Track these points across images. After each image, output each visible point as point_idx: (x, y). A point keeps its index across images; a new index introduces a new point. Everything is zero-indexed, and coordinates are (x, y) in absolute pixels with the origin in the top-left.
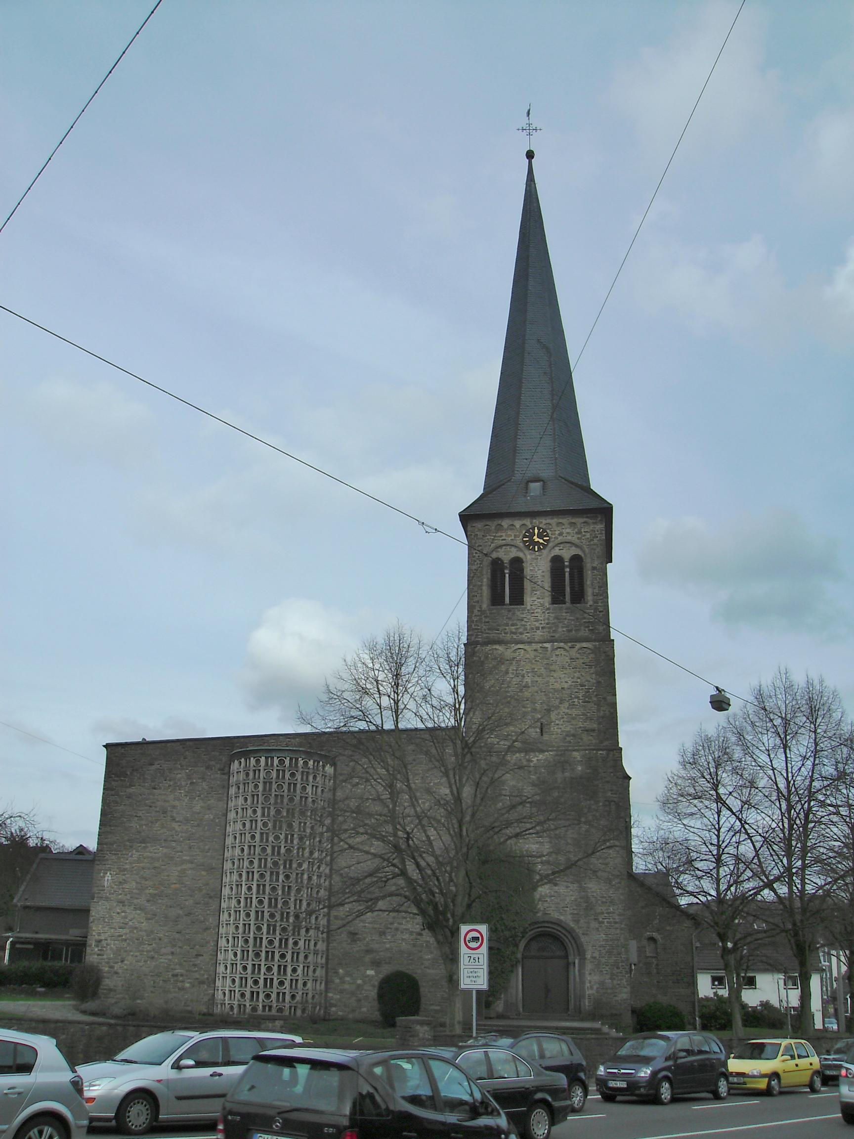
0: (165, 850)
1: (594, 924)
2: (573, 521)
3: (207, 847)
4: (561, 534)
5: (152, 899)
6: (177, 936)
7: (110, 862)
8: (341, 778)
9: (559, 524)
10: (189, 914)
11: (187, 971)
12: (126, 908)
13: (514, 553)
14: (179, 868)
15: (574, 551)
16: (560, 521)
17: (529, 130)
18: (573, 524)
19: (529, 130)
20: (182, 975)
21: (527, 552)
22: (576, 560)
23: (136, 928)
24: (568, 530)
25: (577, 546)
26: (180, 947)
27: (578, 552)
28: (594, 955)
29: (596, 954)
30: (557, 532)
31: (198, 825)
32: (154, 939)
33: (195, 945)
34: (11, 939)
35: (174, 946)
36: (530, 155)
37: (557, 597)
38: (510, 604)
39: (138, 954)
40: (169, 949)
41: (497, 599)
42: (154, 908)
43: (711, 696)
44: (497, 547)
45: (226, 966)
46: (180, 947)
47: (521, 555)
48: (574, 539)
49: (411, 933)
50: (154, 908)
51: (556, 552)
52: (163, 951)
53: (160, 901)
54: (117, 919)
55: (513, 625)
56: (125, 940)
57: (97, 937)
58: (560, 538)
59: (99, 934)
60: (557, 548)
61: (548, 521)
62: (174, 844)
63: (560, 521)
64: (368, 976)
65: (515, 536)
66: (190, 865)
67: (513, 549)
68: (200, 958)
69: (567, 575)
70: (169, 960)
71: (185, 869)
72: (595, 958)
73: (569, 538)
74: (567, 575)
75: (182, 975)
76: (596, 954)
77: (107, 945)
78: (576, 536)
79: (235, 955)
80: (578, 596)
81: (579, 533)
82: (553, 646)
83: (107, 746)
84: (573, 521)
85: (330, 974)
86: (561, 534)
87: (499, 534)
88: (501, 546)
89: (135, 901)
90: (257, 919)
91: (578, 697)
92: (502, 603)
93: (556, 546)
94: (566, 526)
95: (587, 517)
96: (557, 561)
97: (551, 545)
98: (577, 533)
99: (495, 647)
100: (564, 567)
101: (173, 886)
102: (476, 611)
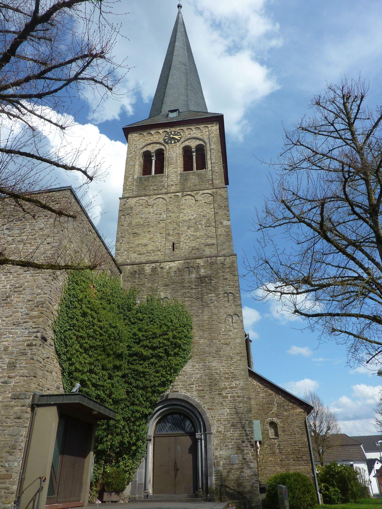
1: (218, 399)
15: (198, 142)
28: (220, 429)
29: (221, 429)
30: (187, 133)
36: (179, 6)
47: (163, 147)
72: (220, 432)
76: (221, 429)
82: (183, 194)
86: (189, 134)
91: (201, 224)
99: (141, 198)
100: (192, 152)
102: (130, 179)
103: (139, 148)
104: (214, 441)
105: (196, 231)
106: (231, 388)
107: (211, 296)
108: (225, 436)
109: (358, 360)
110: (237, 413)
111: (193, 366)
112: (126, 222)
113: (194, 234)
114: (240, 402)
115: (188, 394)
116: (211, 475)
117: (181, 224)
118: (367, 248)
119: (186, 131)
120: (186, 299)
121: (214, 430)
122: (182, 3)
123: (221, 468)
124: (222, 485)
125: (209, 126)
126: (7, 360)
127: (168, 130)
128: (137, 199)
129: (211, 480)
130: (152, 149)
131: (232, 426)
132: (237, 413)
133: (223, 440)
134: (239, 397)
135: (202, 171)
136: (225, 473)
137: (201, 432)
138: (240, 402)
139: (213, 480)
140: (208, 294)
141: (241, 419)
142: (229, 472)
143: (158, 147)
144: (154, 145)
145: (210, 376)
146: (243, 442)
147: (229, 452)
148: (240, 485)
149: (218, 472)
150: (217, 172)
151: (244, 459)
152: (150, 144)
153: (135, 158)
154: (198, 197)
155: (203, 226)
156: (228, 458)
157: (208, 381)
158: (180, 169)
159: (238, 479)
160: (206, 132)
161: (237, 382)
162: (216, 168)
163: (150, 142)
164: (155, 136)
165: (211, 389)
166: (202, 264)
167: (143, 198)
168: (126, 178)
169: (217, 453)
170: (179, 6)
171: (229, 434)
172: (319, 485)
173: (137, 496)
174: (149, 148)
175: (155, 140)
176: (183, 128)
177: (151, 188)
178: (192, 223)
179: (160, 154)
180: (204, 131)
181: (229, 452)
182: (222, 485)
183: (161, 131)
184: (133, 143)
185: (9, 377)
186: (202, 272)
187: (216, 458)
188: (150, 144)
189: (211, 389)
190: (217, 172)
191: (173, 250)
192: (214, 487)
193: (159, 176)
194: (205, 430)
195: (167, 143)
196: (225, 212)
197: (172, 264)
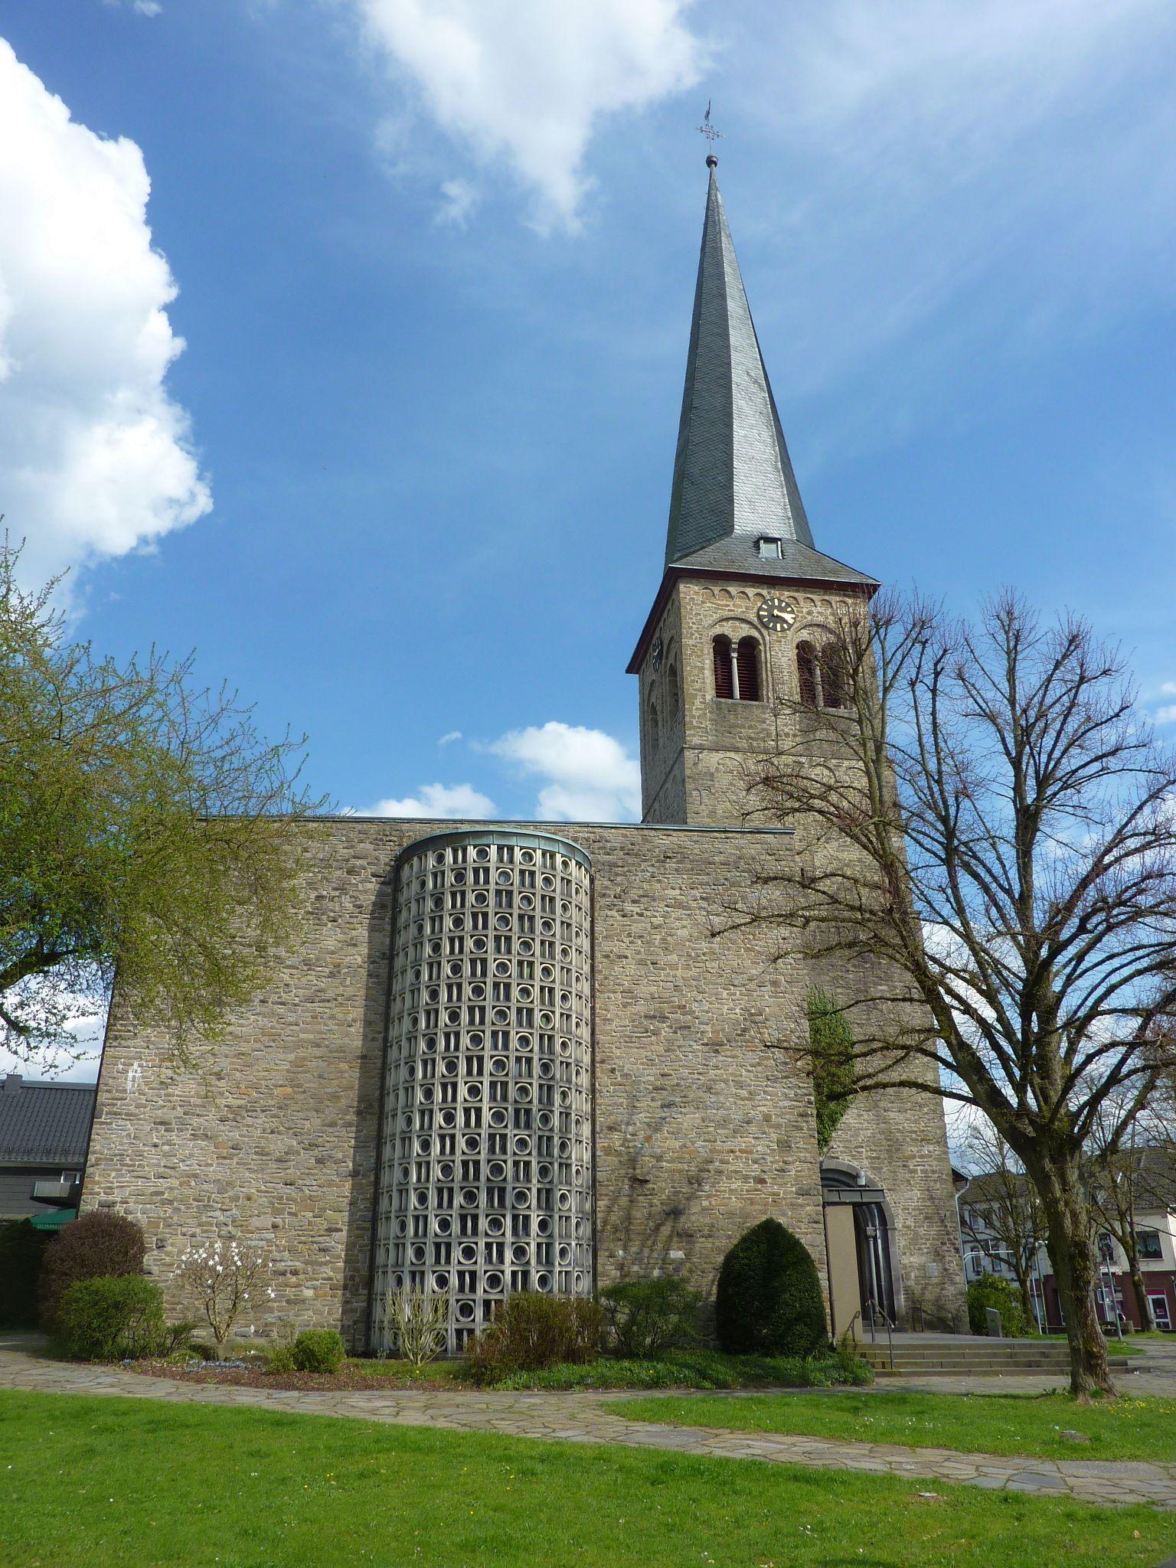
0: (262, 1021)
1: (902, 1174)
3: (350, 1017)
5: (232, 1117)
6: (288, 1190)
8: (603, 901)
10: (313, 1146)
11: (306, 1263)
12: (173, 1136)
14: (291, 1057)
17: (711, 134)
20: (295, 1273)
22: (831, 650)
23: (195, 1176)
28: (908, 1223)
29: (910, 1222)
31: (332, 975)
32: (236, 1199)
33: (324, 1210)
35: (277, 1212)
36: (710, 162)
39: (198, 1230)
40: (268, 1221)
42: (236, 1135)
47: (756, 634)
49: (746, 1178)
50: (236, 1135)
52: (255, 1222)
53: (249, 1121)
54: (152, 1156)
56: (171, 1202)
57: (103, 1197)
59: (109, 1191)
62: (281, 1009)
64: (674, 1261)
66: (316, 1052)
70: (268, 1241)
71: (304, 1059)
72: (908, 1227)
73: (821, 619)
75: (295, 1273)
76: (910, 1222)
83: (628, 671)
85: (600, 1261)
86: (810, 613)
89: (195, 1121)
90: (492, 1150)
92: (731, 696)
94: (819, 604)
96: (804, 648)
99: (729, 754)
103: (705, 624)
104: (899, 1242)
106: (922, 1157)
108: (916, 1233)
110: (932, 1198)
111: (860, 1116)
112: (703, 807)
114: (935, 1181)
115: (855, 1164)
116: (899, 1291)
118: (1046, 849)
119: (802, 604)
120: (839, 990)
121: (899, 1225)
123: (911, 1283)
124: (916, 1308)
125: (850, 601)
126: (774, 1137)
127: (764, 592)
128: (721, 755)
130: (737, 633)
131: (926, 1218)
132: (932, 1198)
133: (915, 1240)
134: (934, 1172)
136: (918, 1290)
137: (874, 1225)
138: (935, 1181)
139: (901, 1301)
140: (876, 984)
141: (938, 1208)
142: (923, 1289)
143: (745, 631)
144: (737, 624)
145: (888, 1135)
146: (944, 1244)
147: (924, 1259)
148: (941, 1308)
149: (907, 1289)
151: (946, 1270)
152: (728, 619)
153: (702, 651)
156: (922, 1267)
157: (884, 1142)
159: (938, 1299)
161: (931, 1148)
163: (727, 614)
164: (738, 602)
165: (891, 1157)
167: (732, 755)
169: (905, 1260)
171: (922, 1231)
174: (726, 629)
175: (738, 612)
176: (796, 595)
177: (745, 732)
179: (749, 647)
181: (924, 1259)
182: (916, 1308)
183: (751, 591)
185: (785, 1162)
187: (905, 1267)
188: (728, 619)
189: (891, 1157)
192: (903, 1311)
193: (757, 707)
194: (884, 1221)
195: (767, 628)
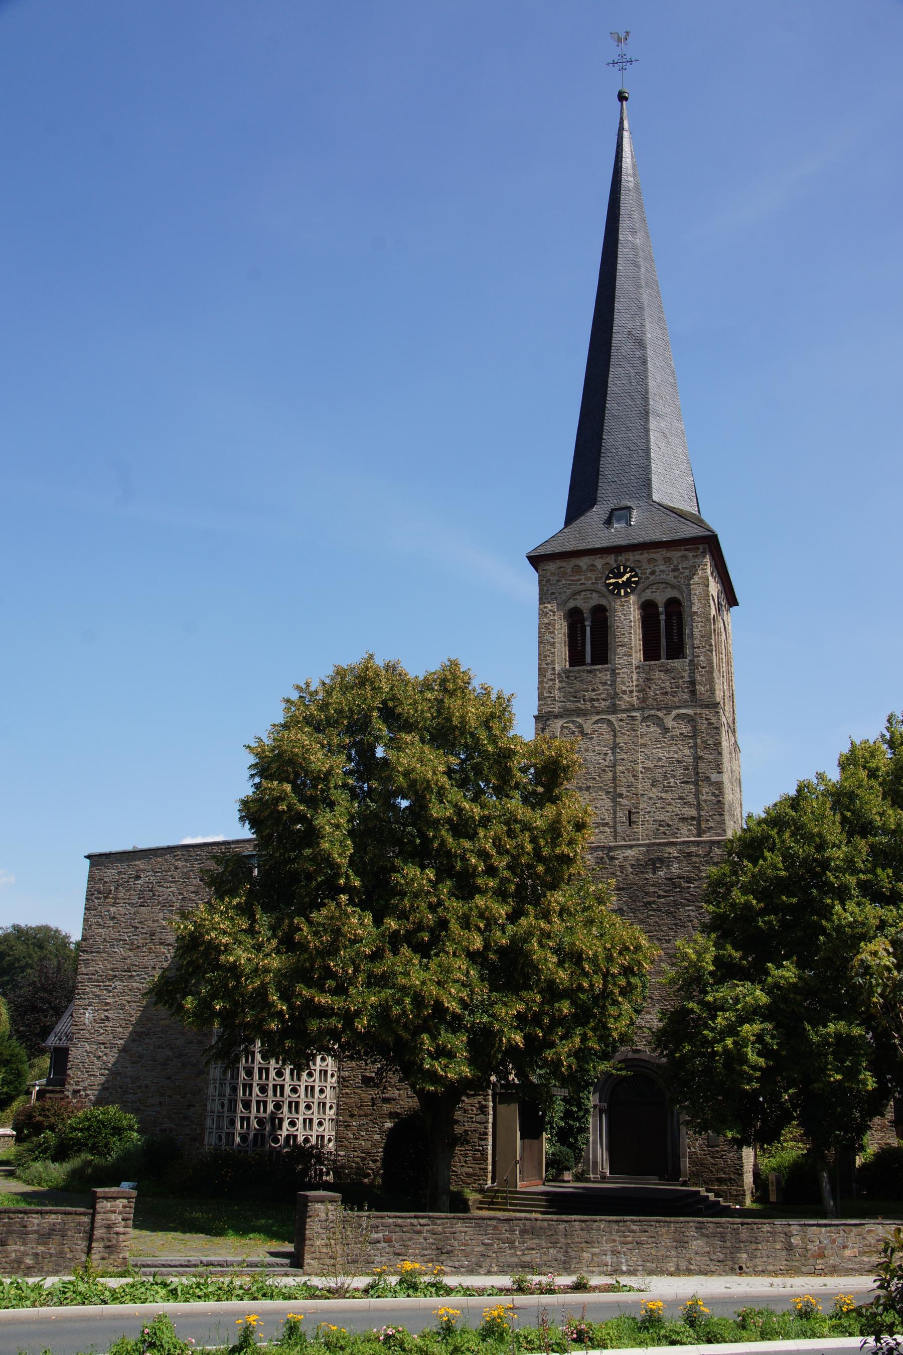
2: (669, 555)
4: (652, 573)
7: (91, 995)
9: (650, 561)
13: (595, 600)
15: (671, 593)
16: (652, 556)
18: (668, 560)
19: (622, 63)
21: (611, 597)
23: (120, 1074)
24: (662, 568)
25: (673, 587)
26: (170, 1096)
27: (675, 594)
30: (648, 571)
32: (140, 1087)
34: (37, 1088)
36: (622, 97)
37: (651, 652)
38: (593, 663)
41: (576, 658)
43: (245, 803)
44: (575, 594)
45: (213, 1119)
46: (170, 1096)
47: (604, 602)
48: (670, 577)
51: (648, 595)
53: (147, 1041)
55: (593, 690)
58: (652, 577)
60: (648, 591)
61: (638, 557)
63: (652, 556)
65: (596, 579)
67: (595, 595)
68: (192, 1109)
69: (662, 623)
73: (663, 576)
74: (662, 623)
77: (87, 1095)
78: (672, 574)
79: (223, 1105)
80: (677, 650)
81: (676, 569)
82: (642, 715)
84: (669, 555)
87: (577, 577)
88: (579, 593)
91: (674, 777)
93: (647, 588)
95: (686, 550)
97: (640, 586)
98: (673, 570)
100: (658, 614)
101: (162, 1022)
102: (549, 675)
105: (667, 791)
107: (689, 910)
109: (403, 1282)
113: (663, 795)
117: (640, 775)
122: (629, 91)
129: (685, 1162)
130: (585, 604)
135: (676, 663)
150: (703, 668)
154: (669, 722)
155: (678, 782)
158: (637, 656)
160: (683, 568)
162: (702, 658)
166: (676, 855)
168: (542, 672)
170: (622, 97)
172: (547, 1171)
173: (591, 1176)
178: (658, 774)
180: (680, 567)
184: (547, 590)
186: (675, 868)
188: (579, 593)
190: (703, 668)
191: (630, 825)
196: (715, 755)
197: (629, 852)
